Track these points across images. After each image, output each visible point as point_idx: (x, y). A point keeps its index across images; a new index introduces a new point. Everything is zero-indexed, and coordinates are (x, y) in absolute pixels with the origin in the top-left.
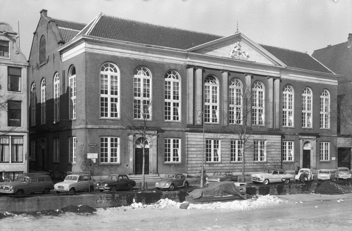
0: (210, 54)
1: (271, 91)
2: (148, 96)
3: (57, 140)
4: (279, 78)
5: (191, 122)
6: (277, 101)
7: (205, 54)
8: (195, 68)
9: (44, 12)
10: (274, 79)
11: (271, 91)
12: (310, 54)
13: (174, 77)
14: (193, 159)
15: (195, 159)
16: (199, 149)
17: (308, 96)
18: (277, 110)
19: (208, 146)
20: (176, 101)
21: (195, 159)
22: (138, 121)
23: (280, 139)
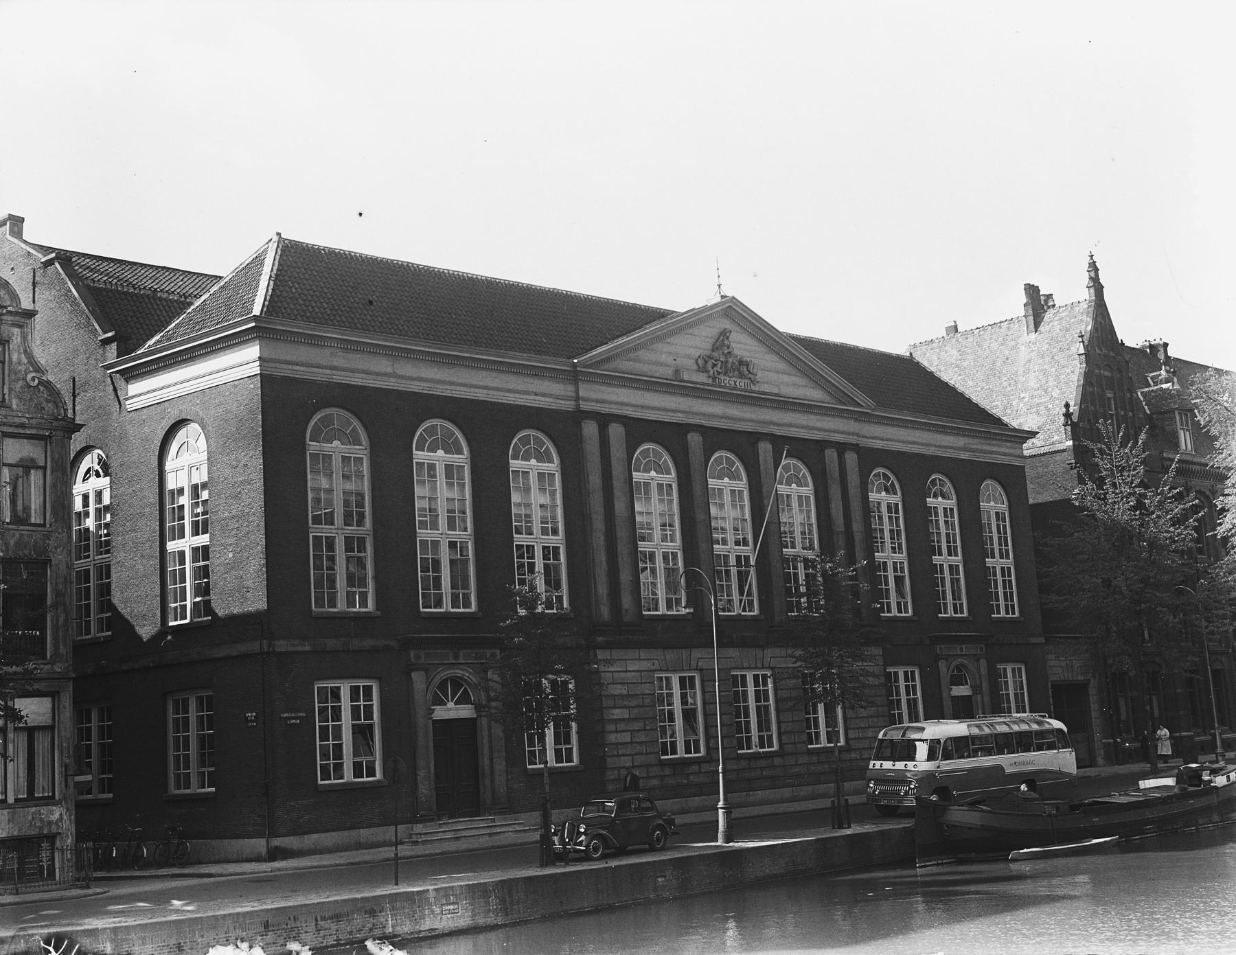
3: (186, 702)
4: (856, 448)
5: (605, 612)
8: (604, 420)
10: (842, 448)
11: (835, 492)
16: (636, 711)
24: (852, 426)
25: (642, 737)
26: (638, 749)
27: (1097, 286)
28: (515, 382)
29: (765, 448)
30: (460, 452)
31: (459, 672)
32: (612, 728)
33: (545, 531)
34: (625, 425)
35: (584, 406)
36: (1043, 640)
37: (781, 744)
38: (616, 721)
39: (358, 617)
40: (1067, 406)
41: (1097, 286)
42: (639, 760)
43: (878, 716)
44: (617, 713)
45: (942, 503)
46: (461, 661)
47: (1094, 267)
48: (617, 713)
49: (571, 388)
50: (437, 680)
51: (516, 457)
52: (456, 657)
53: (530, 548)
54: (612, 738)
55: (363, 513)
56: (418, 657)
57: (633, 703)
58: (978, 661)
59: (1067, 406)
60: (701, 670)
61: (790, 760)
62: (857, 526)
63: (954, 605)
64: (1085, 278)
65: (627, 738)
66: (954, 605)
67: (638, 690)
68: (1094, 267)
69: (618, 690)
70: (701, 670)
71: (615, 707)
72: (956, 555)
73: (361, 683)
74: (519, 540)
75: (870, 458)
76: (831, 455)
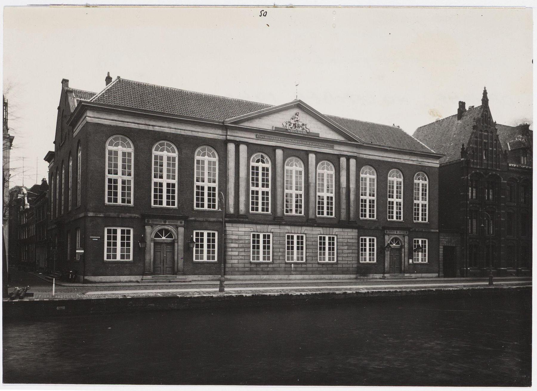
0: (246, 125)
1: (343, 174)
2: (373, 196)
4: (355, 157)
5: (232, 210)
6: (352, 186)
7: (242, 124)
8: (237, 144)
9: (65, 82)
10: (348, 158)
11: (343, 174)
12: (410, 131)
13: (296, 166)
14: (243, 258)
15: (237, 258)
16: (241, 245)
17: (395, 179)
18: (352, 197)
19: (256, 242)
20: (265, 189)
21: (237, 258)
22: (256, 214)
23: (356, 234)
24: (355, 150)
25: (243, 254)
26: (241, 257)
27: (485, 100)
28: (386, 155)
29: (312, 158)
30: (175, 152)
31: (166, 227)
32: (230, 250)
33: (370, 195)
34: (283, 150)
35: (229, 137)
36: (438, 231)
37: (306, 260)
38: (232, 248)
39: (424, 224)
40: (463, 145)
41: (485, 100)
42: (241, 261)
43: (352, 253)
44: (233, 245)
45: (395, 179)
46: (167, 223)
47: (485, 93)
48: (233, 245)
49: (225, 132)
50: (391, 238)
51: (390, 176)
52: (165, 222)
53: (393, 202)
54: (230, 253)
55: (175, 175)
56: (148, 221)
57: (241, 242)
58: (404, 237)
59: (463, 145)
60: (337, 235)
61: (308, 265)
62: (352, 186)
63: (396, 215)
64: (481, 96)
65: (237, 253)
66: (396, 215)
67: (243, 237)
68: (485, 93)
69: (234, 237)
70: (337, 235)
71: (232, 243)
72: (426, 200)
73: (372, 238)
74: (416, 202)
75: (361, 163)
76: (343, 160)
